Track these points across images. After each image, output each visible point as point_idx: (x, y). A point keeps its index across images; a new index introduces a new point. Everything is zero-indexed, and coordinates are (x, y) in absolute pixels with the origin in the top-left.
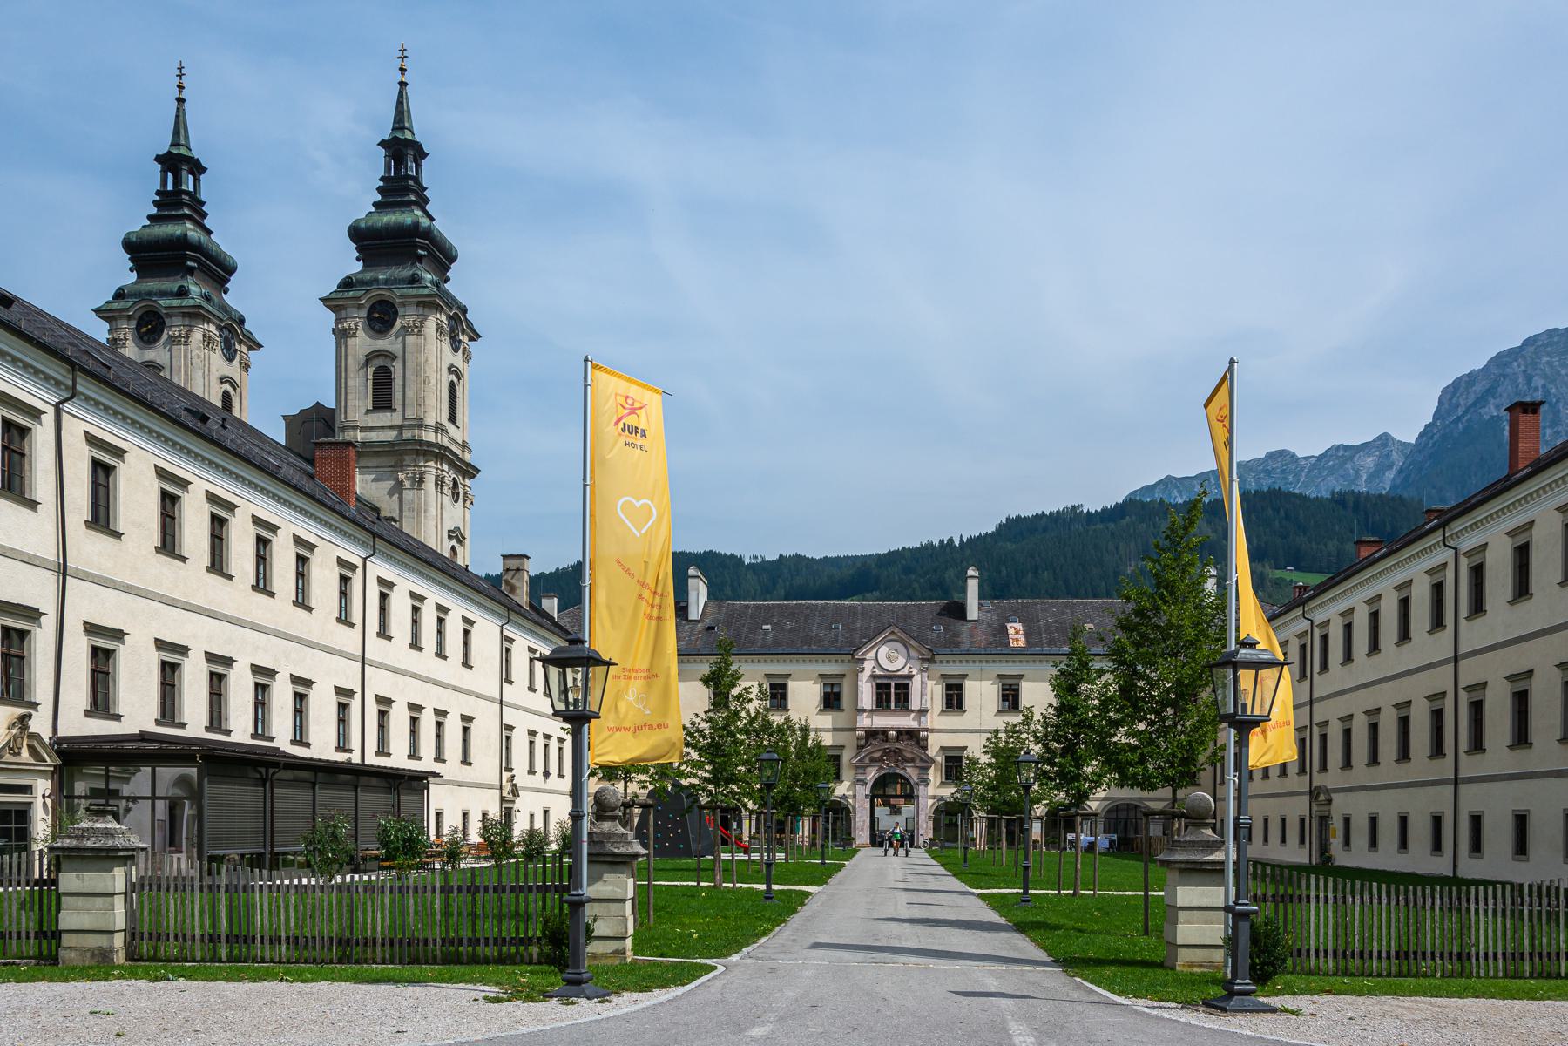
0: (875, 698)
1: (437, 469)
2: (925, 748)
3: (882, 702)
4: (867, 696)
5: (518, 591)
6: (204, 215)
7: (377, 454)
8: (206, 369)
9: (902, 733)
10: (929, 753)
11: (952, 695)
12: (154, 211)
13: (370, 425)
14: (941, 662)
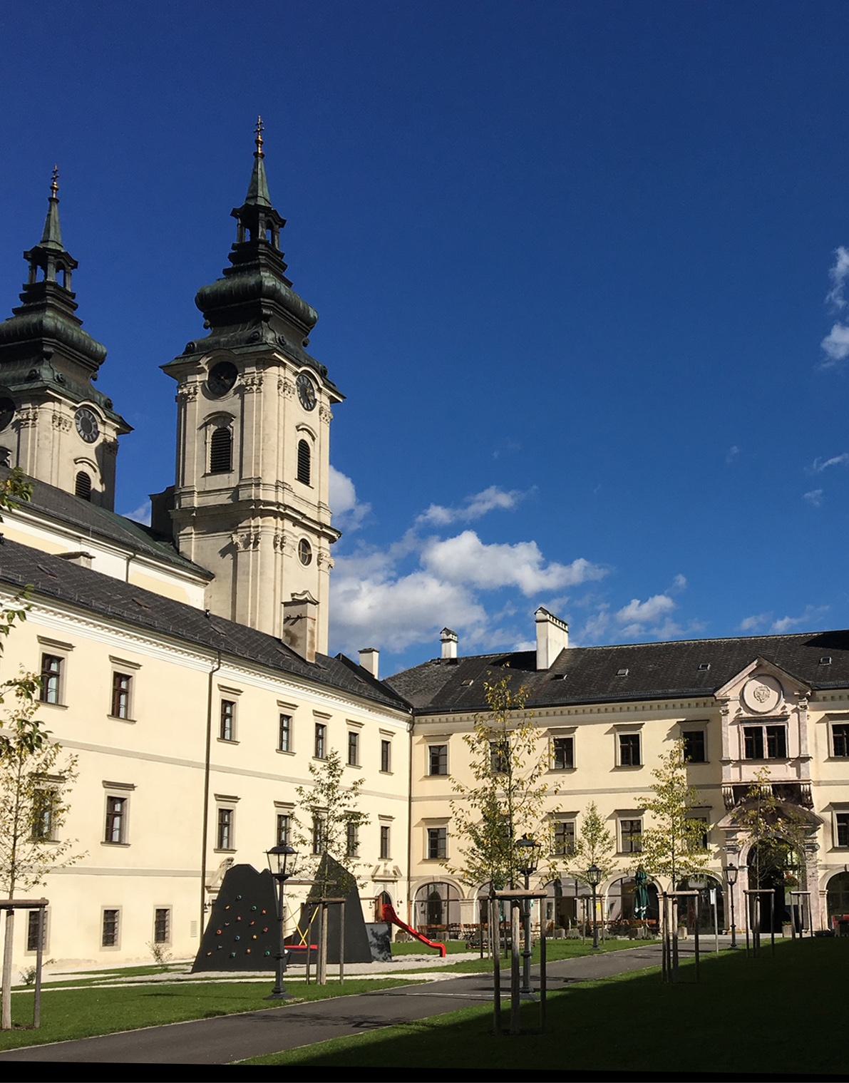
0: (743, 746)
2: (810, 805)
3: (753, 753)
4: (732, 742)
5: (299, 642)
6: (284, 267)
8: (56, 449)
9: (780, 788)
10: (816, 810)
11: (841, 738)
12: (21, 304)
13: (207, 489)
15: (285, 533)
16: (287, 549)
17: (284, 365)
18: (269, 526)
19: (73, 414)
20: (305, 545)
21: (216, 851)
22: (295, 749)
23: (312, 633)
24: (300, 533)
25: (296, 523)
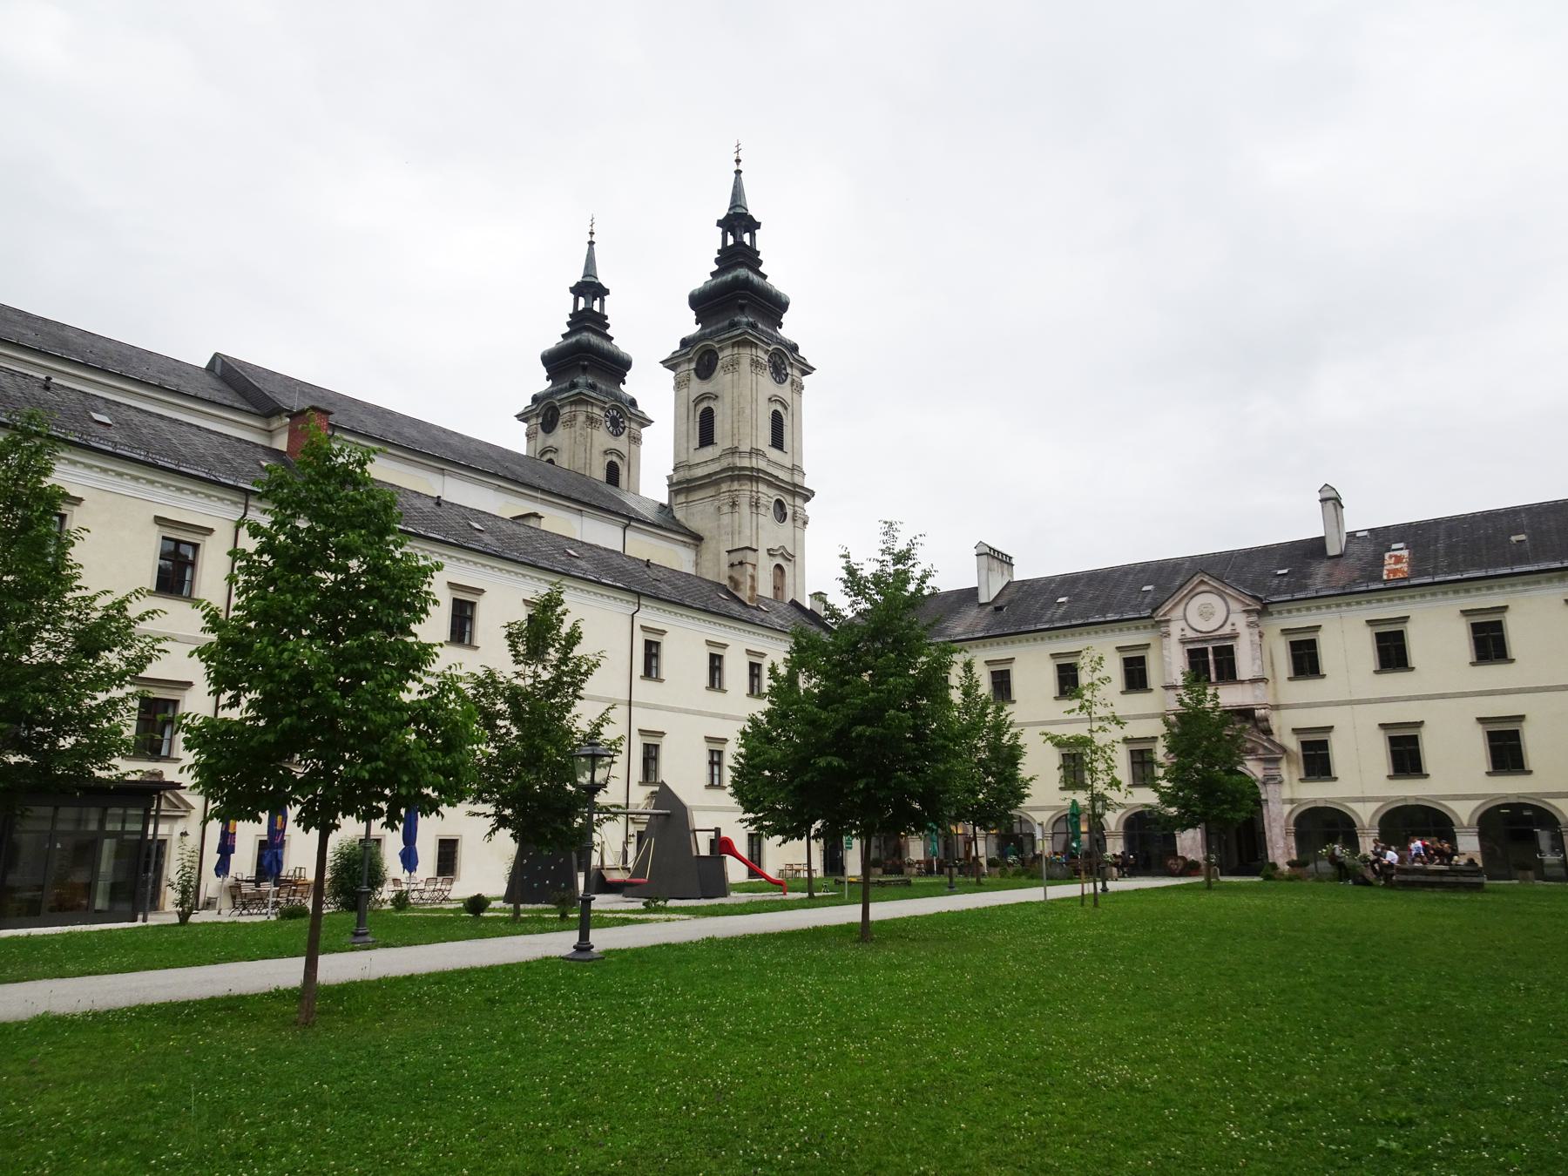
1: (751, 491)
5: (742, 587)
7: (701, 487)
14: (1280, 612)
15: (760, 495)
16: (762, 510)
17: (756, 346)
18: (745, 490)
19: (603, 414)
20: (779, 503)
21: (641, 784)
22: (726, 686)
23: (752, 577)
24: (774, 494)
25: (770, 484)
